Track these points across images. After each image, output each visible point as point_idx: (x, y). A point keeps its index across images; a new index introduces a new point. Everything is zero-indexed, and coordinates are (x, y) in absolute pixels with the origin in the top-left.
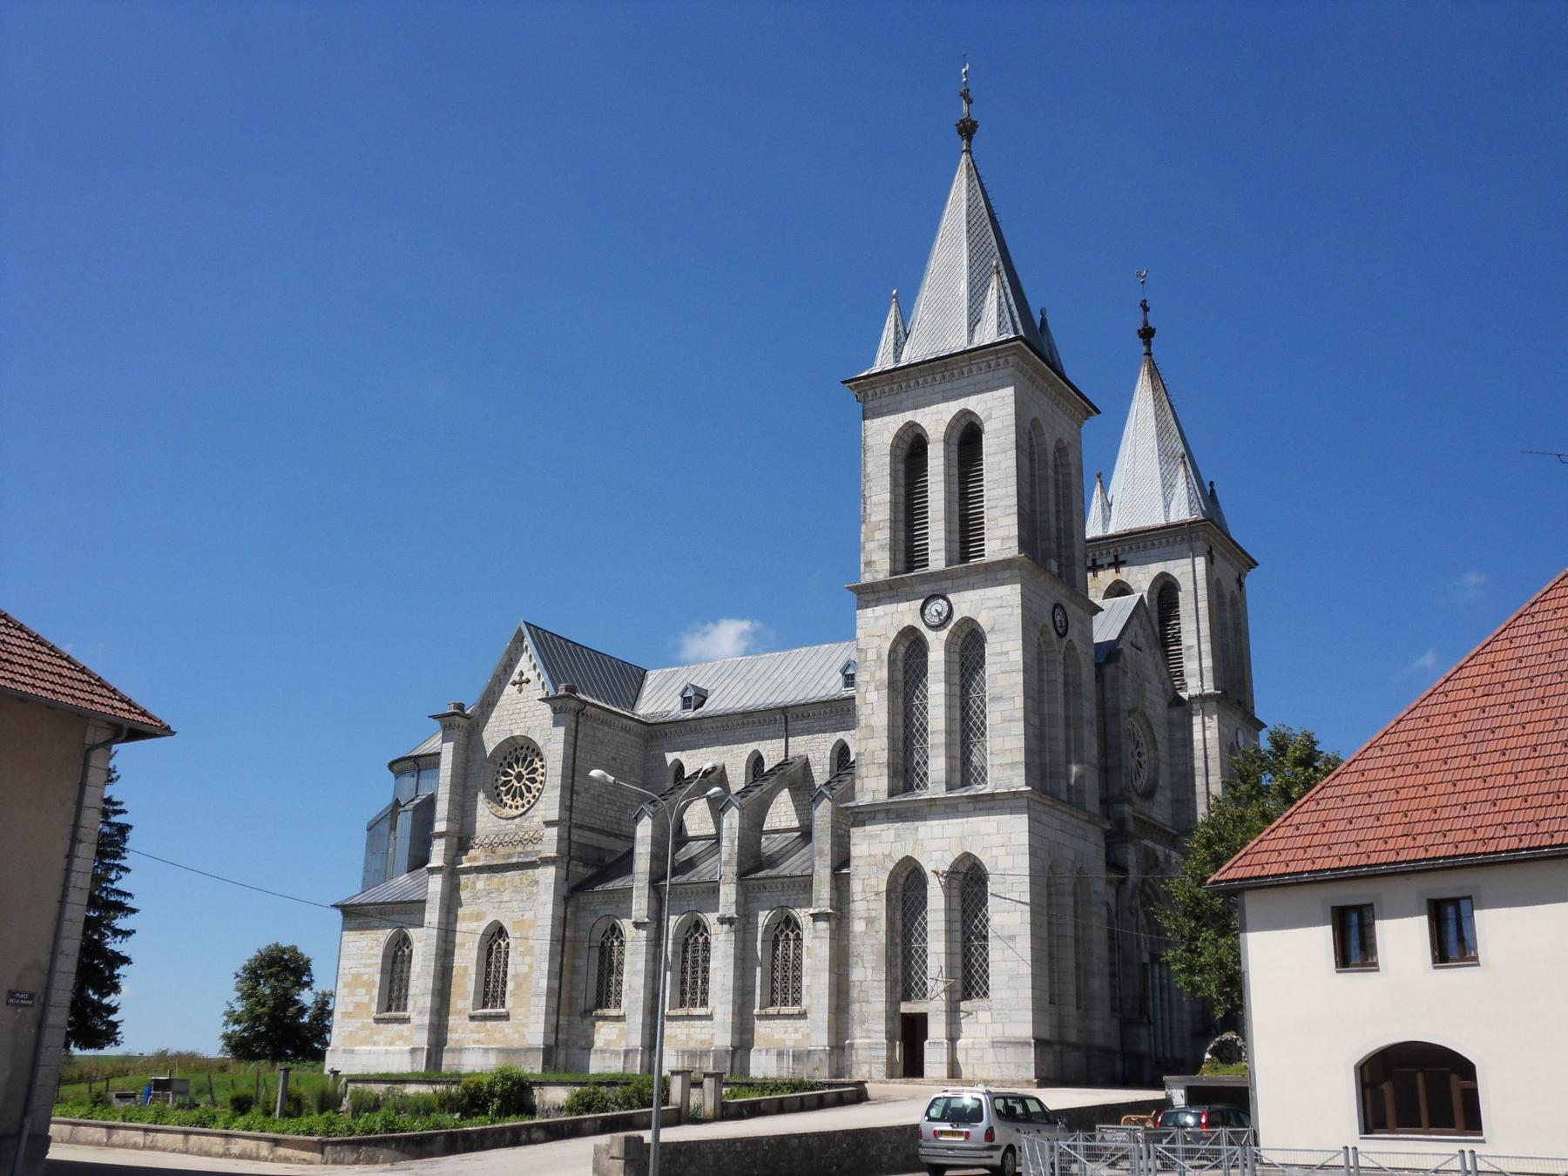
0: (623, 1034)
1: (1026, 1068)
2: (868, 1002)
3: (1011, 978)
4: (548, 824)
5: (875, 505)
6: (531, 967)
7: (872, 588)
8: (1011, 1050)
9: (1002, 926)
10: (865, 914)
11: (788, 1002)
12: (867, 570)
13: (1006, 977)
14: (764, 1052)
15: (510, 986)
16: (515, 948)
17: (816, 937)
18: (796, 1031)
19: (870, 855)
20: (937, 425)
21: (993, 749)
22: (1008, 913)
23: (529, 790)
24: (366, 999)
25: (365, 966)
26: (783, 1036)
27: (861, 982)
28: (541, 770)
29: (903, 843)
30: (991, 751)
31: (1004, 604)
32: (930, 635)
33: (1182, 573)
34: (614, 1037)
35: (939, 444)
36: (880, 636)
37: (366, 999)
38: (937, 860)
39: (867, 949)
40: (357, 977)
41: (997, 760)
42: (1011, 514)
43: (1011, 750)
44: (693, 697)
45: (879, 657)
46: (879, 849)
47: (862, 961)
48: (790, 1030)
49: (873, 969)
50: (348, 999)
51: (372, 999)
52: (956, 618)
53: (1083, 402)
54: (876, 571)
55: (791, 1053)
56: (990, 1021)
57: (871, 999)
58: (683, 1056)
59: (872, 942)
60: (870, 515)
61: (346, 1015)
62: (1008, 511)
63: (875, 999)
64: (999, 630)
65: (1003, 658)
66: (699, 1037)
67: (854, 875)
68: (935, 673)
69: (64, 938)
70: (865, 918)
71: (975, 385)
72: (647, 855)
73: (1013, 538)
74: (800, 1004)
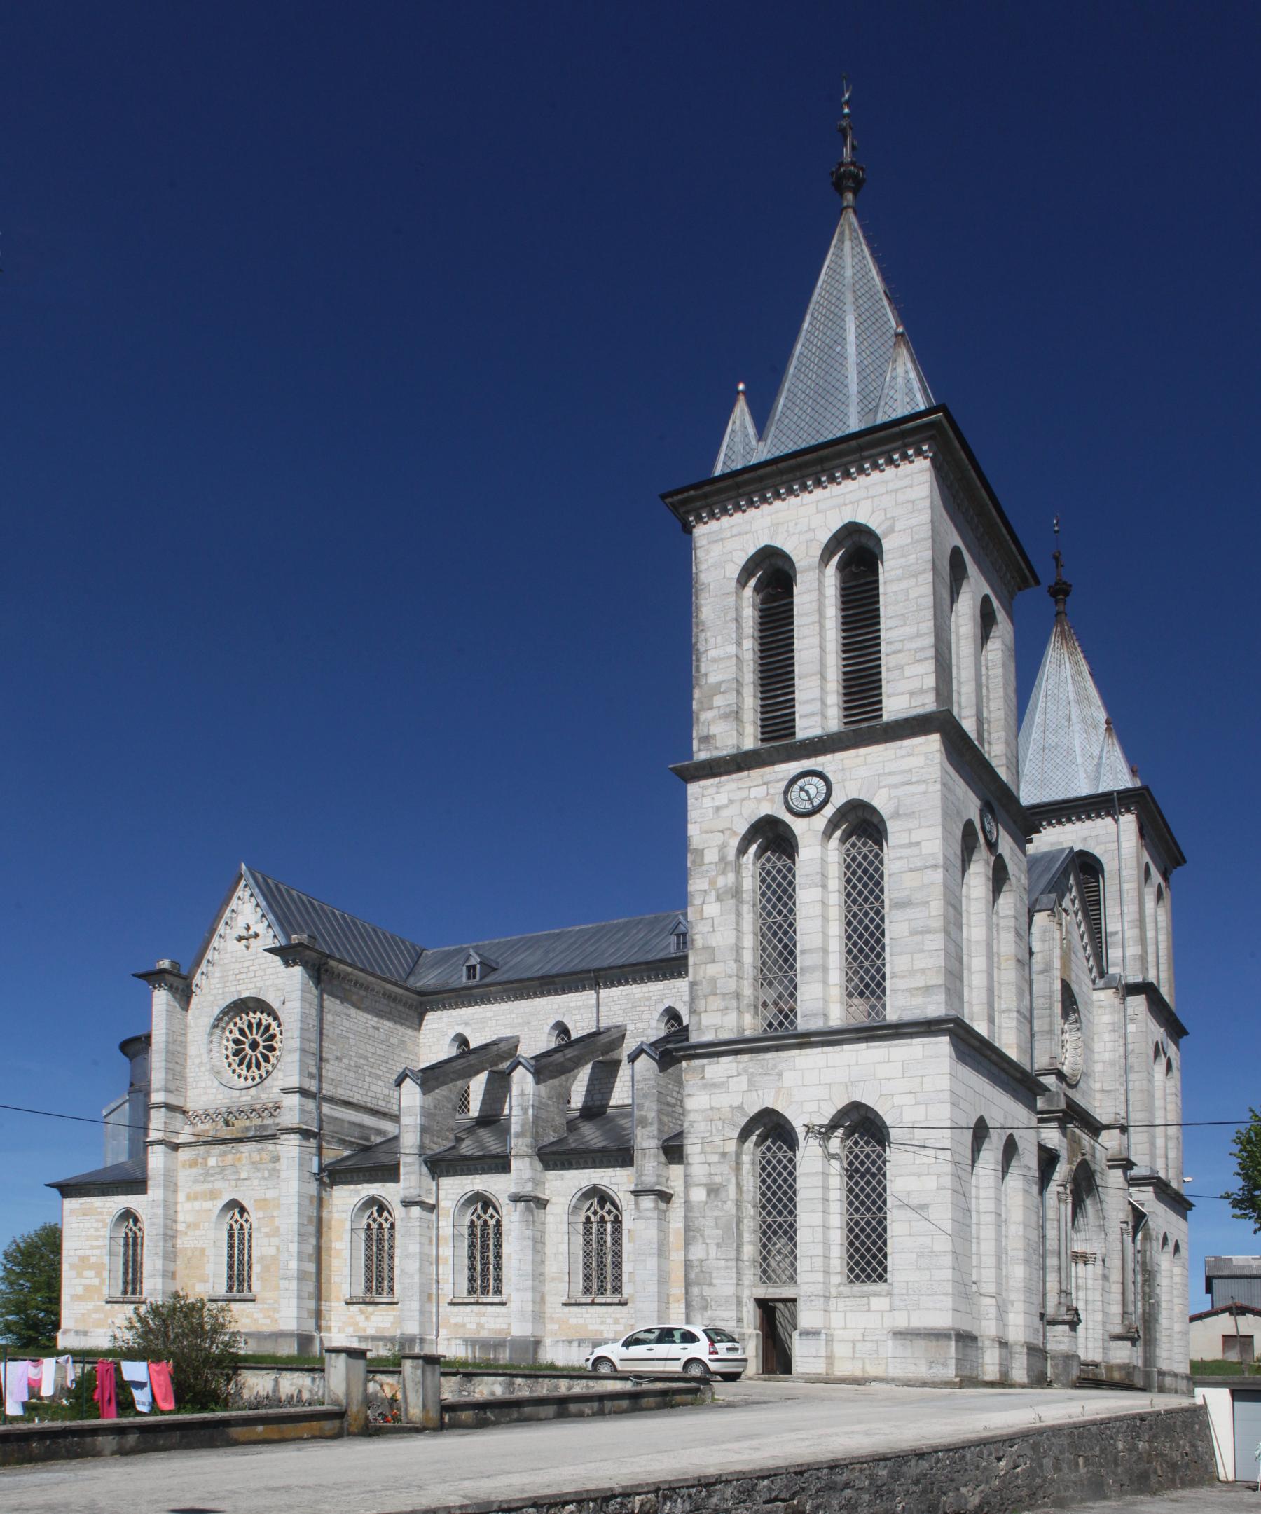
0: (400, 1320)
1: (943, 1365)
2: (710, 1284)
3: (921, 1255)
4: (287, 1091)
5: (715, 661)
6: (278, 1248)
7: (711, 768)
8: (921, 1344)
9: (909, 1192)
10: (704, 1180)
11: (605, 1290)
12: (702, 747)
13: (914, 1256)
14: (576, 1344)
15: (256, 1269)
16: (259, 1229)
17: (639, 1218)
18: (616, 1321)
19: (712, 1108)
20: (807, 547)
21: (896, 970)
22: (919, 1176)
23: (267, 1059)
24: (96, 1282)
25: (92, 1247)
26: (602, 1327)
27: (702, 1261)
28: (229, 1052)
30: (892, 973)
31: (914, 780)
32: (799, 826)
33: (1106, 851)
34: (388, 1325)
35: (811, 573)
36: (722, 832)
37: (96, 1282)
38: (810, 1113)
39: (710, 1222)
40: (84, 1259)
41: (902, 984)
42: (926, 659)
43: (923, 971)
44: (478, 966)
45: (722, 859)
46: (724, 1100)
47: (702, 1236)
48: (609, 1320)
49: (718, 1245)
50: (77, 1281)
51: (102, 1282)
52: (838, 800)
53: (1019, 558)
54: (717, 748)
56: (888, 1308)
57: (715, 1281)
58: (473, 1346)
59: (717, 1213)
60: (706, 675)
61: (76, 1298)
62: (919, 656)
63: (723, 1281)
64: (905, 815)
65: (915, 850)
66: (492, 1326)
67: (689, 1133)
68: (807, 876)
69: (1116, 821)
70: (705, 1185)
71: (867, 488)
72: (415, 1127)
73: (927, 691)
74: (620, 1293)
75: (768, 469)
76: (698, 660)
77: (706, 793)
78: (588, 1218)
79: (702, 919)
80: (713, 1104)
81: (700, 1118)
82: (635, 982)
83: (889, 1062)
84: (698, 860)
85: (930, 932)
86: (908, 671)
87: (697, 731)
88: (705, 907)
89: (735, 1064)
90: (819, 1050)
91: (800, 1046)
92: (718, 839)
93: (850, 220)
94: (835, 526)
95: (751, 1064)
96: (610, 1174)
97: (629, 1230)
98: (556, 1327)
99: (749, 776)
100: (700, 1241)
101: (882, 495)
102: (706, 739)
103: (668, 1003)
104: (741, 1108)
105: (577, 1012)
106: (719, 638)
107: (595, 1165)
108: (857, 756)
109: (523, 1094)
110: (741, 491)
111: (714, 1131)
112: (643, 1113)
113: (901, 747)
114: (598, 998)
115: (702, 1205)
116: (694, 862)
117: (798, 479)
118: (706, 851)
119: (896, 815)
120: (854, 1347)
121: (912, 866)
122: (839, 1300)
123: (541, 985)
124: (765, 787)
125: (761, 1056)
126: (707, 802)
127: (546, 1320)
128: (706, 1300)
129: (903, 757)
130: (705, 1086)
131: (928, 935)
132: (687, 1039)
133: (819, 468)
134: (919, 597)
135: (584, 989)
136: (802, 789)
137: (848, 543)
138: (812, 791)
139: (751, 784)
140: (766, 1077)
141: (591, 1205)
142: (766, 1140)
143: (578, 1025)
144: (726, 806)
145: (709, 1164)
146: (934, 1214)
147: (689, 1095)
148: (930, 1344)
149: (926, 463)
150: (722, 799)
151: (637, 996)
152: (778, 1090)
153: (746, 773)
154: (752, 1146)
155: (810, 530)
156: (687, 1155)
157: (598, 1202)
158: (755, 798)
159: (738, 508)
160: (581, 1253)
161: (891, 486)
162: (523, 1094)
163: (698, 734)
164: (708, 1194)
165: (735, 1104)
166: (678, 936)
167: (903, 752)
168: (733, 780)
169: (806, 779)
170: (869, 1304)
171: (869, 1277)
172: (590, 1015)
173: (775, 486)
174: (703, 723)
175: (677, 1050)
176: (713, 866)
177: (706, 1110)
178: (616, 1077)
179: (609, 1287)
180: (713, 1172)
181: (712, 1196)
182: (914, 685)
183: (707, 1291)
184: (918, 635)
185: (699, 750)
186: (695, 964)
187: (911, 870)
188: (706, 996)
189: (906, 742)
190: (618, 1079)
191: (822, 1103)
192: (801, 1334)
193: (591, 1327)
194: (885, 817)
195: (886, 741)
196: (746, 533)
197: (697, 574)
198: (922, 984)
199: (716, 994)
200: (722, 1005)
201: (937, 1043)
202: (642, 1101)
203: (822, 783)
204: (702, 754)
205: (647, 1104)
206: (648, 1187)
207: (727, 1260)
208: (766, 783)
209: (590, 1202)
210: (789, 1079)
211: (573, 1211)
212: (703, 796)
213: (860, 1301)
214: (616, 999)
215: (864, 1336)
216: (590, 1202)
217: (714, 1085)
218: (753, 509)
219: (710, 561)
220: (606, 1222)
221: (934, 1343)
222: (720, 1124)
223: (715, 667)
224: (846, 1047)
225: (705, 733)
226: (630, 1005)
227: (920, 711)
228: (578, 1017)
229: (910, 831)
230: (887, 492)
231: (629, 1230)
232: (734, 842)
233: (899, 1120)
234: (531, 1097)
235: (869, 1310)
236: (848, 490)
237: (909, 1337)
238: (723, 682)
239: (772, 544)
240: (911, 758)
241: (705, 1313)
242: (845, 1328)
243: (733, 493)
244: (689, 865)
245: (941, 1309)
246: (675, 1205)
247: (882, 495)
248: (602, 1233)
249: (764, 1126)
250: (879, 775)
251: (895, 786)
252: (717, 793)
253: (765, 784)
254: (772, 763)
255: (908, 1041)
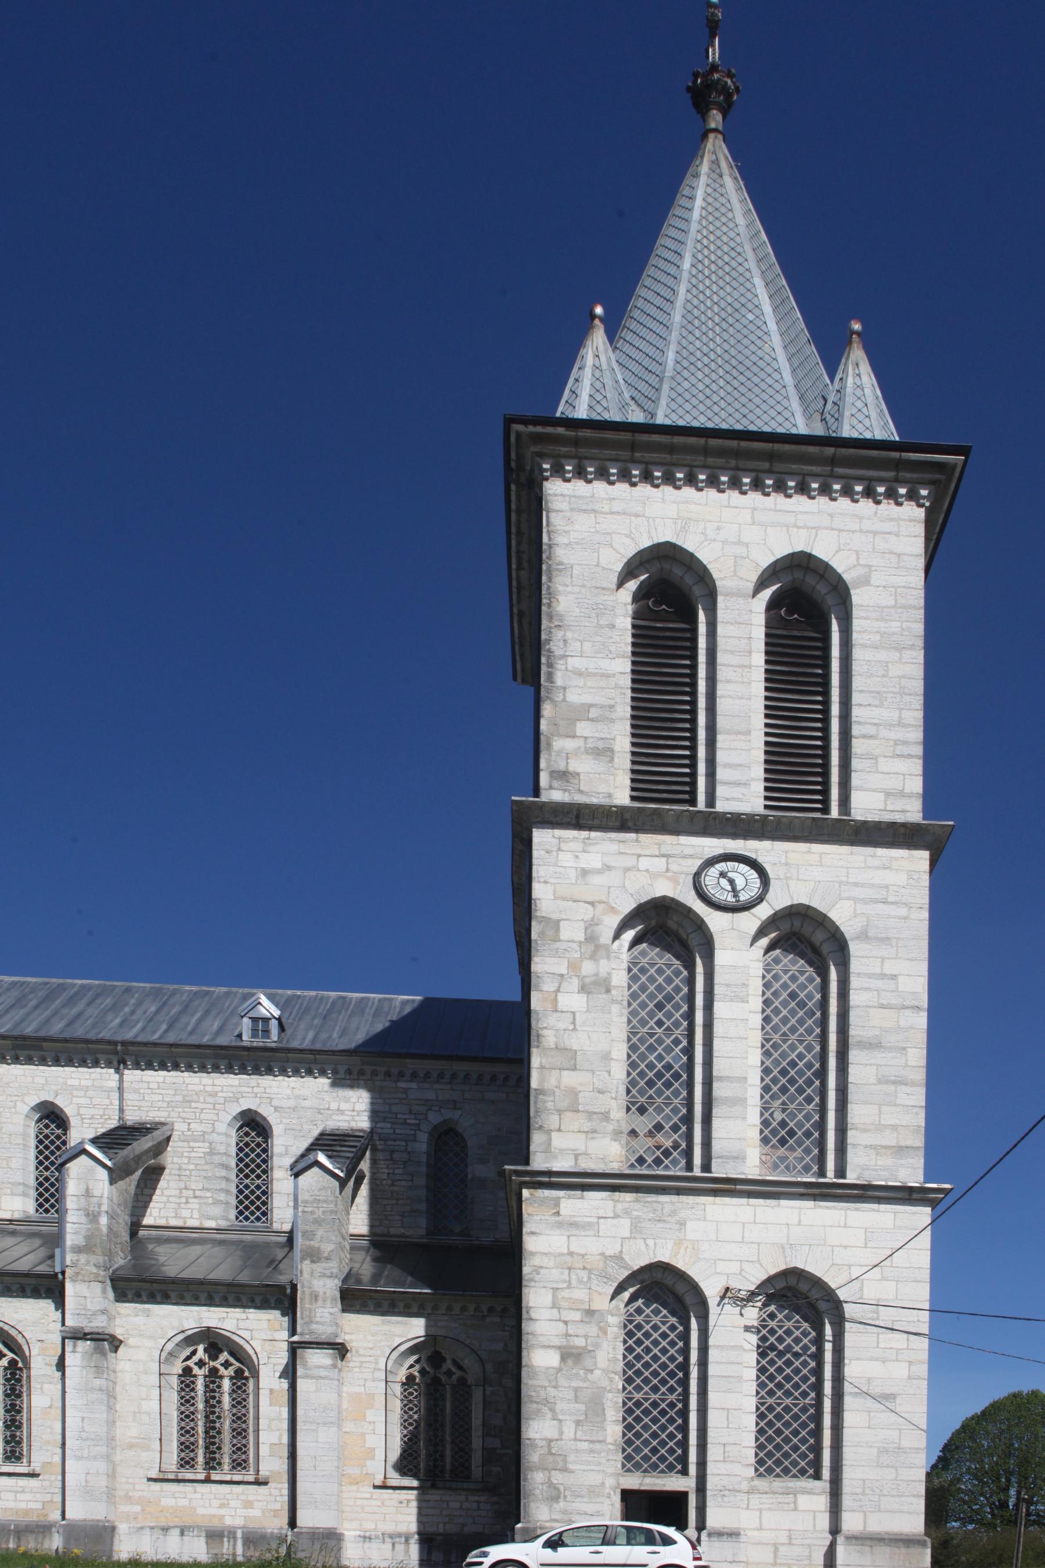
2: (565, 1470)
5: (579, 674)
9: (869, 1379)
10: (557, 1342)
12: (555, 784)
13: (876, 1450)
14: (177, 1531)
18: (248, 1504)
19: (571, 1254)
26: (222, 1512)
27: (551, 1441)
29: (650, 1242)
31: (891, 899)
32: (715, 921)
36: (592, 904)
43: (894, 1128)
45: (591, 938)
46: (589, 1245)
47: (552, 1410)
49: (578, 1423)
52: (778, 900)
55: (239, 1534)
57: (571, 1466)
59: (575, 1384)
60: (565, 689)
65: (890, 985)
68: (728, 985)
70: (559, 1348)
71: (831, 515)
73: (910, 796)
75: (692, 440)
76: (550, 665)
77: (563, 846)
78: (187, 1371)
79: (556, 1011)
80: (573, 1249)
81: (551, 1264)
82: (189, 1068)
83: (845, 1226)
84: (550, 933)
85: (906, 1084)
86: (884, 765)
87: (548, 761)
88: (560, 997)
89: (611, 1202)
90: (744, 1201)
91: (715, 1193)
92: (586, 912)
93: (715, 149)
94: (782, 550)
95: (637, 1206)
96: (238, 1316)
97: (271, 1391)
98: (137, 1508)
99: (637, 841)
100: (549, 1415)
101: (853, 532)
102: (563, 776)
103: (245, 1105)
104: (618, 1258)
105: (82, 1094)
106: (587, 646)
107: (210, 1301)
108: (809, 852)
109: (88, 1194)
110: (637, 455)
111: (574, 1282)
112: (314, 1243)
113: (874, 856)
114: (121, 1081)
115: (553, 1372)
116: (542, 934)
117: (731, 469)
118: (562, 924)
119: (863, 936)
120: (776, 1551)
121: (885, 1002)
122: (751, 1496)
123: (15, 1047)
124: (664, 859)
125: (652, 1198)
126: (566, 859)
127: (117, 1499)
128: (558, 1489)
129: (878, 868)
130: (560, 1225)
131: (903, 1087)
132: (527, 1163)
133: (766, 465)
134: (904, 677)
135: (96, 1064)
136: (723, 875)
137: (787, 578)
138: (740, 883)
139: (639, 851)
140: (660, 1225)
141: (194, 1353)
142: (637, 1300)
143: (83, 1111)
144: (599, 872)
145: (566, 1323)
146: (902, 1405)
147: (533, 1233)
148: (897, 1550)
149: (921, 513)
150: (592, 860)
151: (190, 1087)
152: (679, 1243)
153: (633, 835)
154: (622, 1305)
155: (739, 543)
156: (529, 1309)
157: (205, 1350)
158: (647, 871)
159: (625, 476)
160: (175, 1414)
161: (867, 525)
162: (88, 1194)
163: (548, 766)
164: (564, 1358)
165: (609, 1252)
166: (255, 1020)
167: (876, 862)
168: (612, 840)
169: (742, 866)
170: (795, 1503)
171: (786, 1471)
172: (107, 1102)
173: (691, 466)
174: (559, 753)
175: (518, 1173)
176: (575, 946)
177: (561, 1254)
178: (155, 1189)
179: (226, 1460)
180: (571, 1332)
181: (570, 1362)
182: (893, 784)
183: (557, 1478)
184: (900, 724)
185: (551, 788)
186: (542, 1067)
187: (883, 1007)
188: (560, 1112)
189: (881, 852)
190: (158, 1192)
191: (745, 1266)
192: (710, 1535)
193: (201, 1511)
194: (847, 936)
195: (852, 843)
196: (637, 516)
197: (550, 546)
198: (894, 1143)
199: (578, 1111)
200: (587, 1126)
201: (914, 1213)
202: (313, 1227)
203: (753, 875)
204: (553, 794)
205: (320, 1233)
206: (323, 1338)
207: (592, 1442)
208: (667, 856)
209: (191, 1349)
210: (694, 1230)
211: (167, 1359)
212: (559, 849)
213: (781, 1498)
214: (155, 1086)
215: (790, 1539)
216: (191, 1349)
217: (574, 1225)
218: (649, 487)
219: (573, 535)
220: (221, 1377)
221: (903, 1550)
222: (584, 1275)
223: (581, 682)
224: (784, 1203)
225: (562, 766)
226: (179, 1098)
227: (899, 818)
228: (83, 1101)
229: (883, 959)
230: (861, 531)
231: (271, 1391)
232: (614, 921)
233: (858, 1296)
234: (105, 1201)
235: (795, 1509)
236: (801, 509)
237: (868, 1542)
238: (591, 705)
239: (679, 543)
240: (887, 871)
241: (555, 1505)
242: (761, 1529)
243: (625, 454)
244: (534, 936)
245: (909, 1513)
246: (351, 1364)
247: (853, 532)
248: (214, 1391)
249: (642, 1282)
250: (841, 883)
251: (865, 901)
252: (584, 851)
253: (663, 856)
254: (677, 832)
255: (875, 1206)
